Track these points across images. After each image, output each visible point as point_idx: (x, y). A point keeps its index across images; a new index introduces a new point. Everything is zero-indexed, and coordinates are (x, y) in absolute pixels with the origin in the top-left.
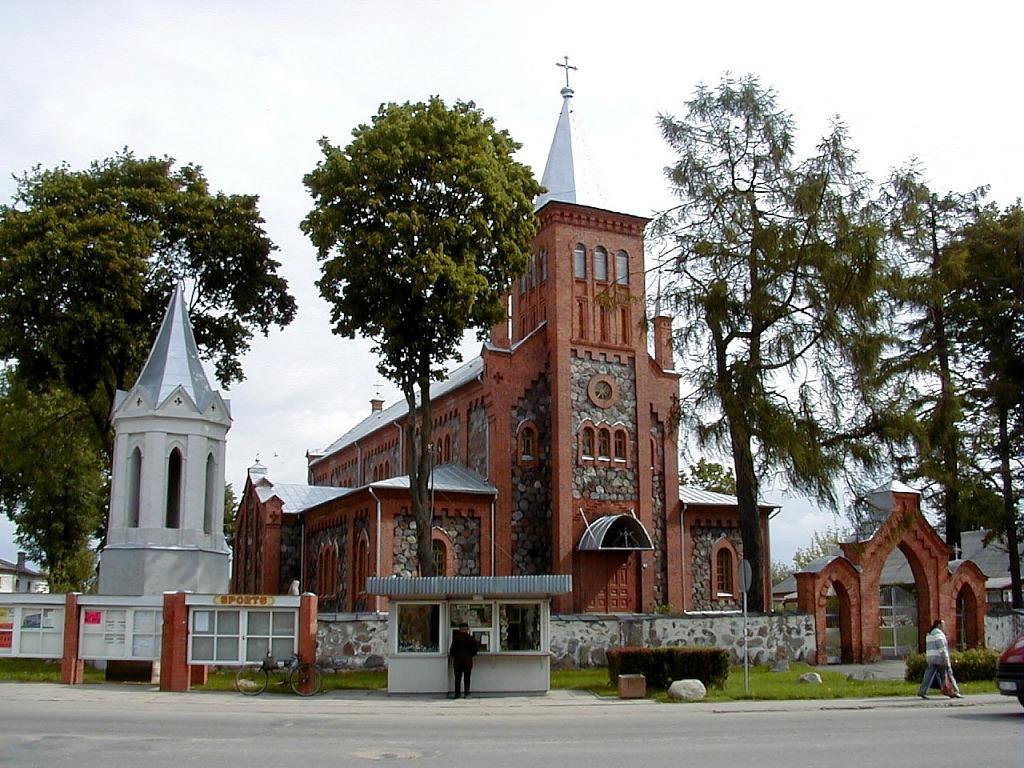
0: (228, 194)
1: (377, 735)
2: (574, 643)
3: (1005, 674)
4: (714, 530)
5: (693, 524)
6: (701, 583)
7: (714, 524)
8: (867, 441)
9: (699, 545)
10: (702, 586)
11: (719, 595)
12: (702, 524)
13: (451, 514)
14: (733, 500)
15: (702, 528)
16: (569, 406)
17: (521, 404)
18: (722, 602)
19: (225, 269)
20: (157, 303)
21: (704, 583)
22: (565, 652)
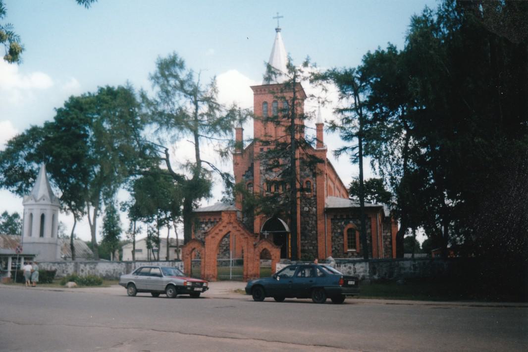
0: (61, 105)
1: (230, 332)
2: (114, 270)
3: (31, 257)
4: (345, 220)
5: (333, 217)
6: (338, 245)
7: (345, 217)
8: (191, 124)
9: (337, 227)
10: (338, 247)
11: (349, 250)
12: (338, 217)
13: (212, 220)
14: (359, 206)
15: (339, 219)
16: (259, 172)
17: (247, 173)
18: (350, 254)
19: (371, 191)
20: (38, 142)
21: (340, 245)
22: (112, 273)
